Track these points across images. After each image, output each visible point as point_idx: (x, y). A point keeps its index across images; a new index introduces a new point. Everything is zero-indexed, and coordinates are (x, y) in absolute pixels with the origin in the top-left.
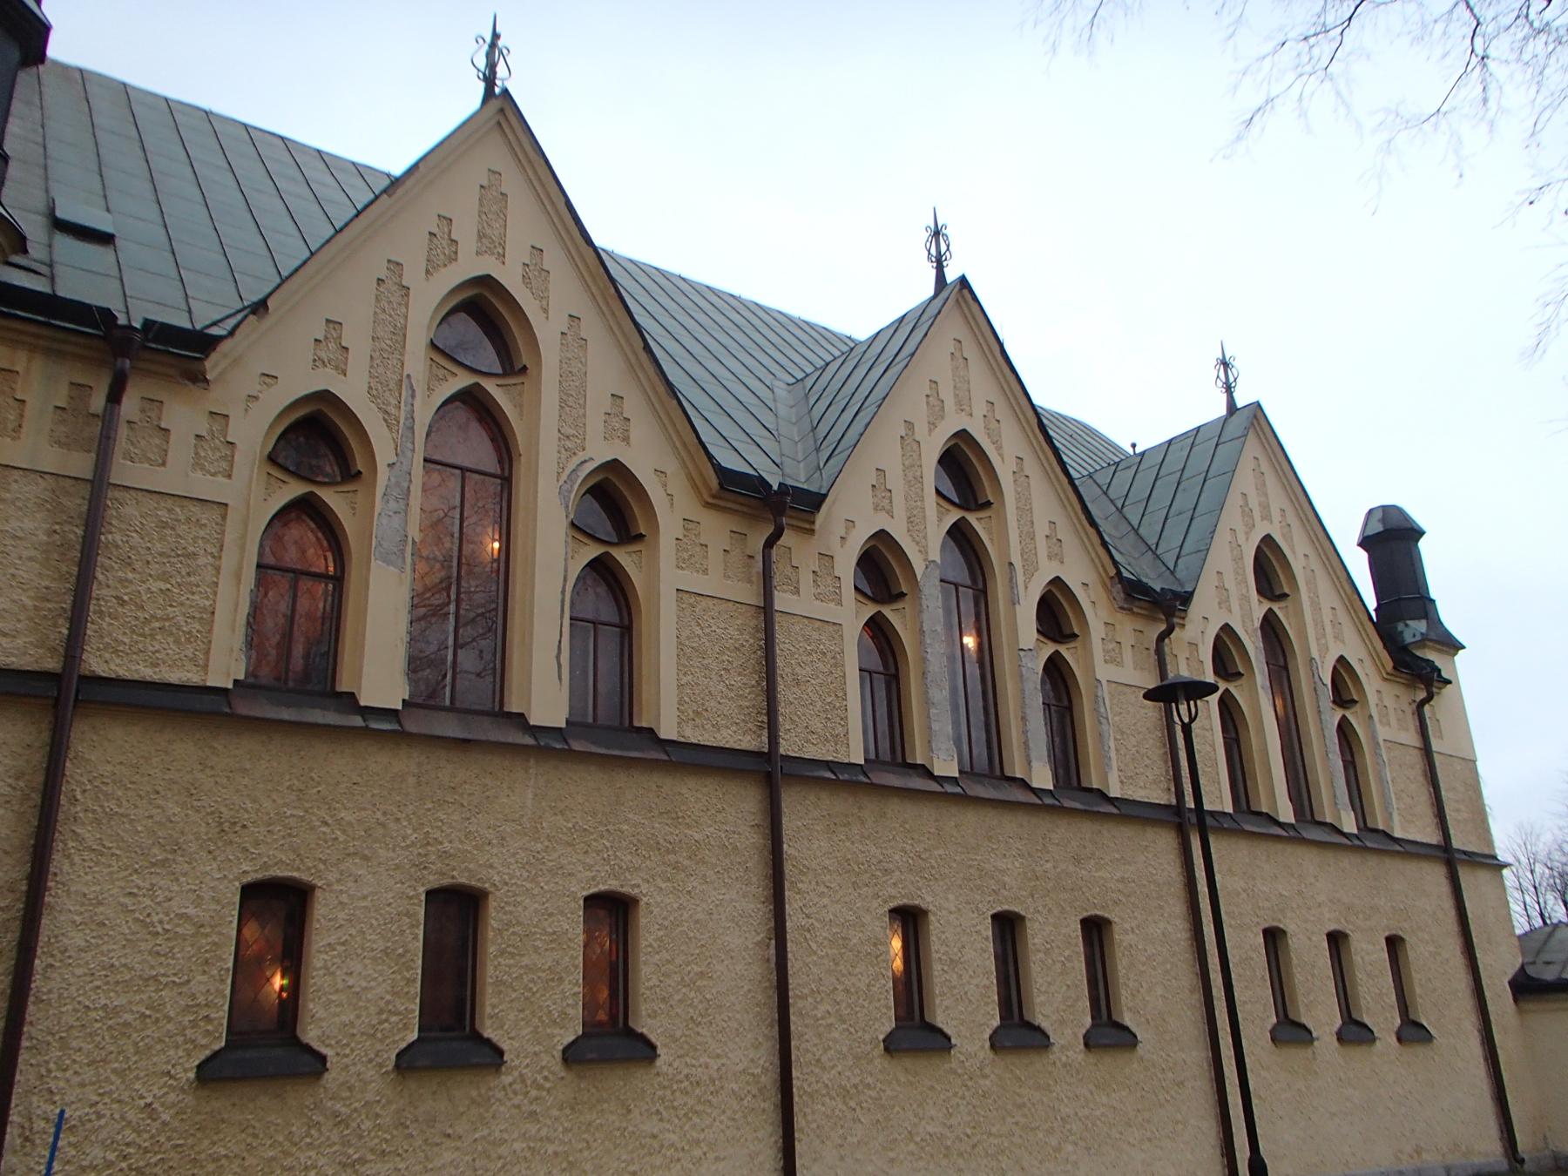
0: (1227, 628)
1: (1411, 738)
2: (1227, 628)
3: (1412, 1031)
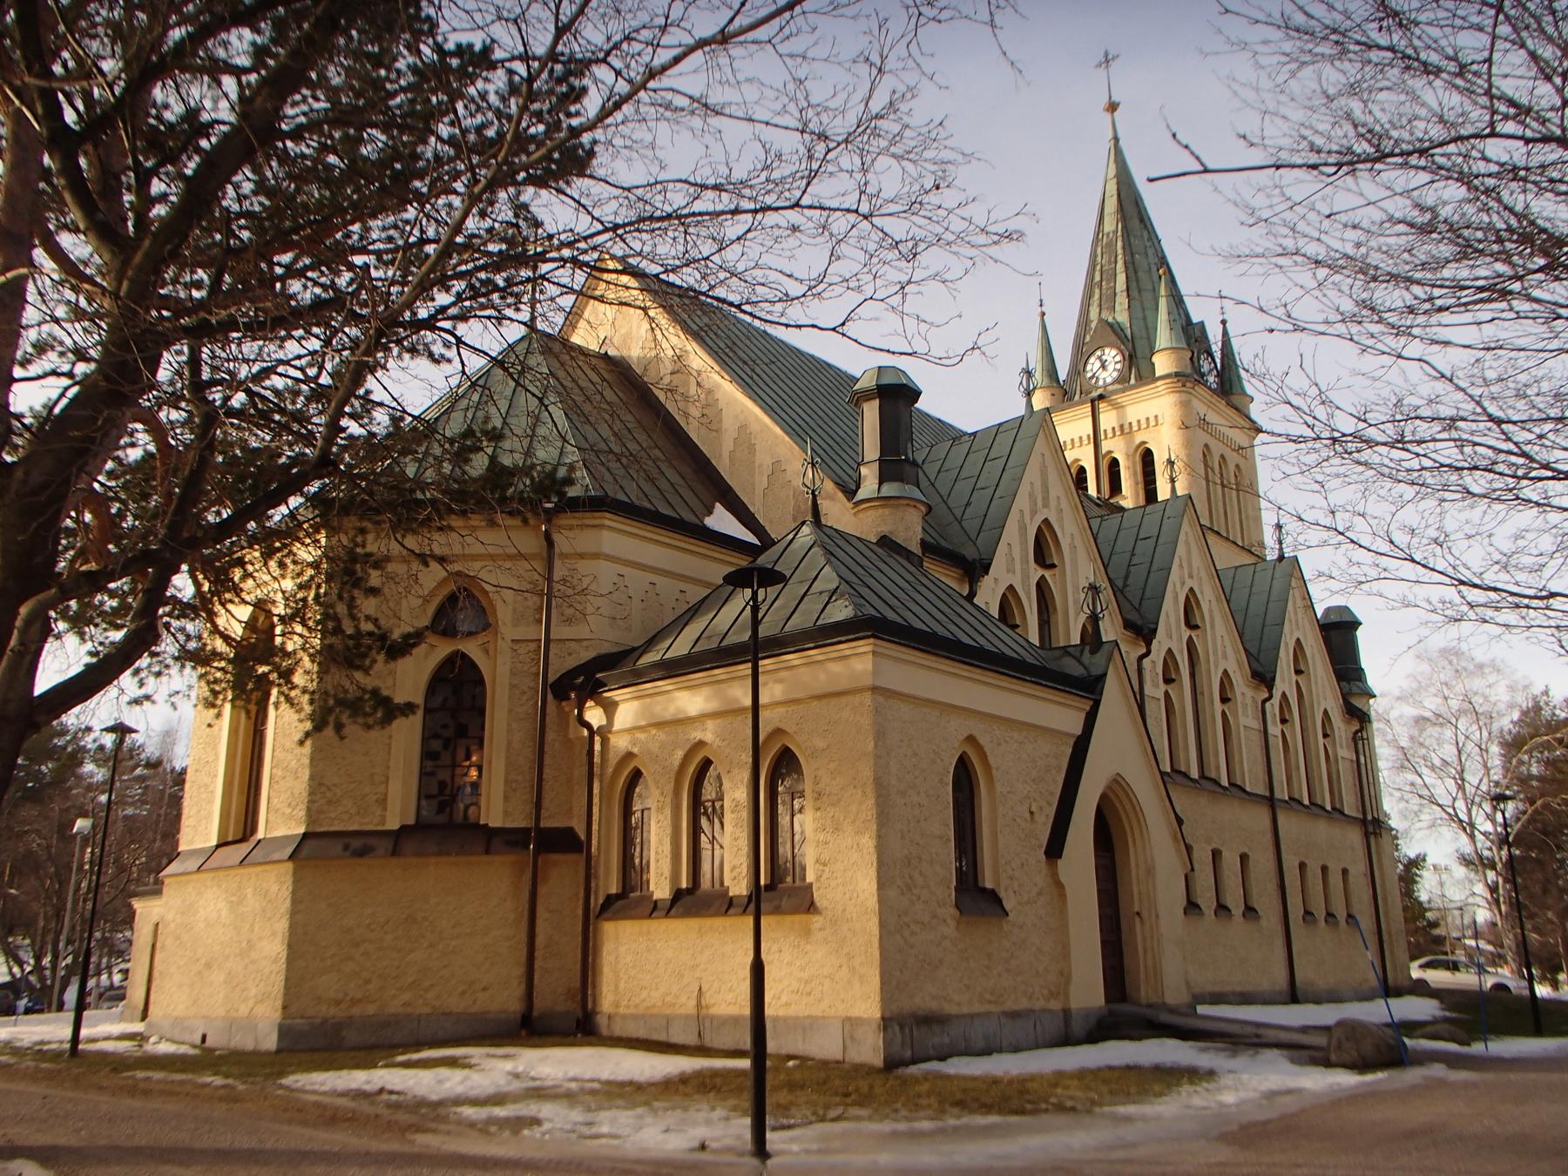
0: (1011, 588)
1: (1256, 724)
2: (1011, 588)
3: (1250, 911)
